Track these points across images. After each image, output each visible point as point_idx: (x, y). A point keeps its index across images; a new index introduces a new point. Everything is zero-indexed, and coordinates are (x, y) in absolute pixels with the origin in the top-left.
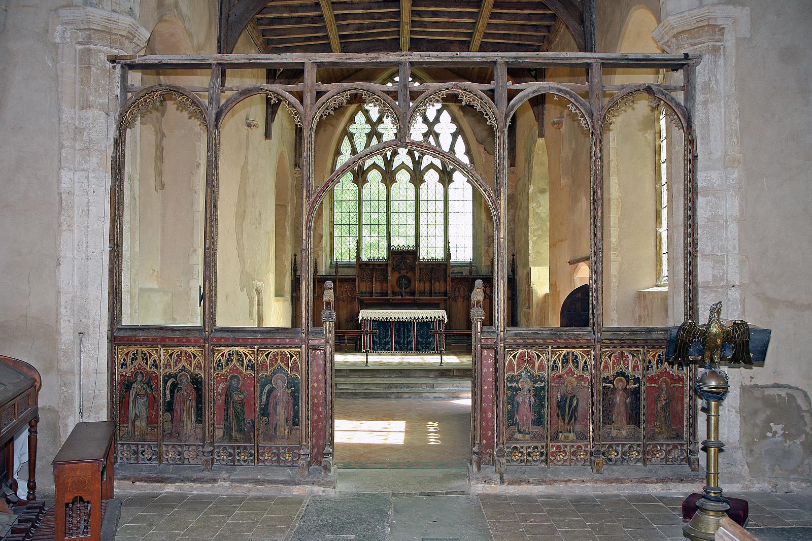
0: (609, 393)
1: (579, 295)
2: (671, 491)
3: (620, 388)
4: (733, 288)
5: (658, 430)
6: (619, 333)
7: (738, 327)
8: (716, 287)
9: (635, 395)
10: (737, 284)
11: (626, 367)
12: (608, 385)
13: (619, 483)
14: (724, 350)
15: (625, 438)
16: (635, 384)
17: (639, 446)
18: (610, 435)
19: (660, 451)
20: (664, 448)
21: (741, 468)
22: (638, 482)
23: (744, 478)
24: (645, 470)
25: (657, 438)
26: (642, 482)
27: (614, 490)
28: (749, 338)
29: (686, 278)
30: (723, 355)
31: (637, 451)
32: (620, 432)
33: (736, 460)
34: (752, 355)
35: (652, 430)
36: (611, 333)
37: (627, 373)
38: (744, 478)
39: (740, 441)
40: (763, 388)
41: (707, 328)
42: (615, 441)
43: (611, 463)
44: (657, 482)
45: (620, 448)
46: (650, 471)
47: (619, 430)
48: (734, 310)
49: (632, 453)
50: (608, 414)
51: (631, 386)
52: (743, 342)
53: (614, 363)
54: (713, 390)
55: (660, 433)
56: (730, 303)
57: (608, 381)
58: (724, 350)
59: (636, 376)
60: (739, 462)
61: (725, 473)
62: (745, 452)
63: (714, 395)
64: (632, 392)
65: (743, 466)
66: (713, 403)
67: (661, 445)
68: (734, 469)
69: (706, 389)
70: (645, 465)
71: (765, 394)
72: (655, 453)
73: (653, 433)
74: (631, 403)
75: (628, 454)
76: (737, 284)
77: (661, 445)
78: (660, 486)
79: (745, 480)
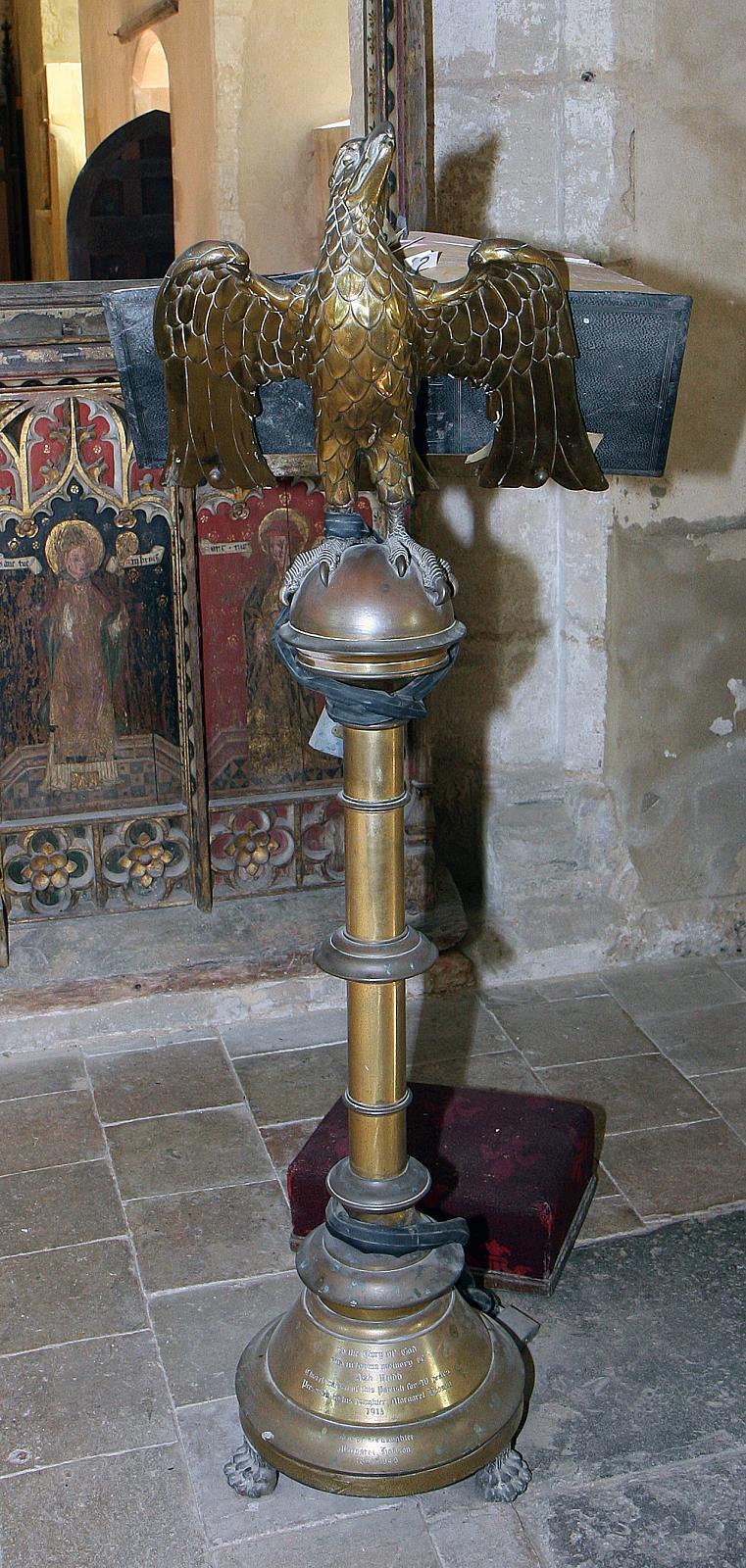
0: (24, 600)
1: (132, 151)
2: (312, 1008)
3: (77, 569)
4: (584, 86)
5: (262, 745)
6: (54, 311)
7: (505, 289)
8: (515, 80)
9: (148, 601)
10: (604, 63)
11: (97, 472)
12: (17, 564)
13: (82, 1004)
14: (447, 418)
15: (117, 795)
16: (144, 549)
17: (173, 822)
18: (43, 788)
19: (273, 834)
20: (290, 820)
21: (608, 872)
22: (170, 987)
23: (617, 914)
24: (200, 930)
25: (258, 782)
26: (185, 986)
27: (61, 1036)
28: (574, 349)
29: (374, 38)
30: (447, 442)
31: (167, 846)
32: (89, 767)
33: (588, 844)
34: (595, 440)
35: (233, 745)
36: (14, 313)
37: (101, 504)
38: (617, 914)
39: (606, 765)
40: (703, 534)
41: (314, 299)
42: (68, 812)
43: (52, 910)
44: (254, 978)
45: (89, 842)
46: (224, 930)
47: (81, 760)
48: (589, 191)
49: (145, 858)
50: (25, 696)
51: (129, 556)
52: (539, 371)
53: (37, 459)
54: (367, 669)
55: (271, 757)
56: (571, 155)
57: (13, 544)
58: (447, 418)
59: (149, 514)
60: (598, 849)
61: (545, 902)
62: (623, 808)
63: (368, 698)
64: (135, 587)
65: (615, 865)
66: (373, 736)
67: (278, 810)
68: (578, 880)
69: (323, 663)
70: (206, 902)
71: (712, 558)
72: (250, 845)
73: (239, 763)
74: (132, 636)
75: (128, 864)
76: (604, 63)
77: (278, 810)
78: (265, 994)
79: (619, 917)
